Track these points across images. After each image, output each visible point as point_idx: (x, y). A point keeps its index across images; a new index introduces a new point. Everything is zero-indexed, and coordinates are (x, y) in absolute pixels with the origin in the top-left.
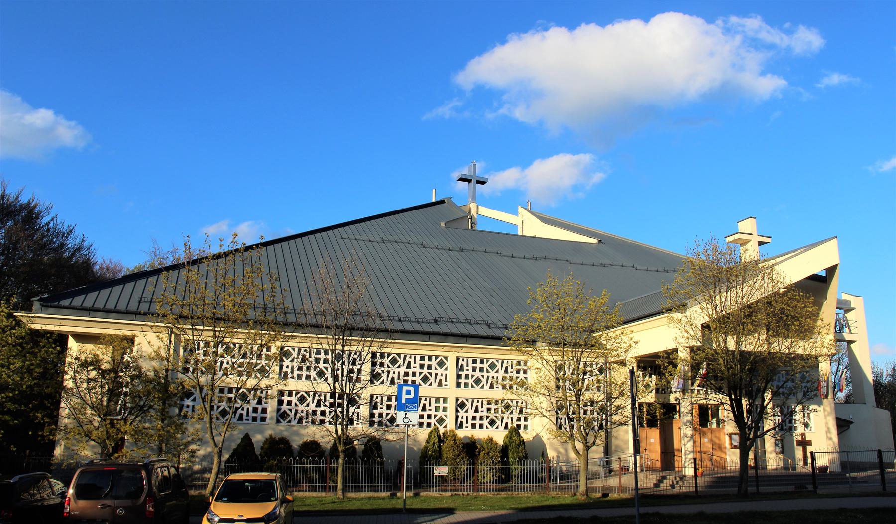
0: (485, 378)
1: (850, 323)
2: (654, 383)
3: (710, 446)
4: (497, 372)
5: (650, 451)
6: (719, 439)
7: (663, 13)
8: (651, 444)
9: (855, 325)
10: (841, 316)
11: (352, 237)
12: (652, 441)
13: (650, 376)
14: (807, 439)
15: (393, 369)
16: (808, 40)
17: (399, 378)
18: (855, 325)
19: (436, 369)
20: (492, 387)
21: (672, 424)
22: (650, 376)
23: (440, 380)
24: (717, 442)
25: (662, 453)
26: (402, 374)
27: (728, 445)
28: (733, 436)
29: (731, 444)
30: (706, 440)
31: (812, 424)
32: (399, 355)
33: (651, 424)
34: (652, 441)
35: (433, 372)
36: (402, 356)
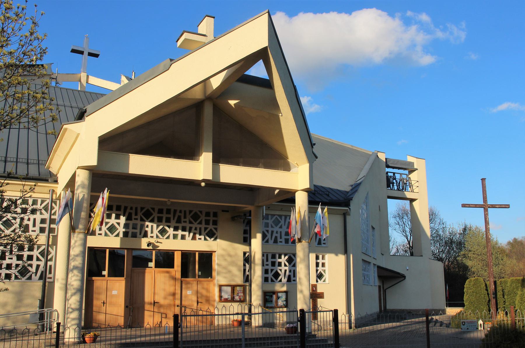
0: (270, 232)
1: (413, 182)
2: (122, 225)
3: (194, 298)
4: (281, 227)
5: (111, 303)
6: (208, 290)
7: (327, 12)
8: (113, 296)
9: (417, 184)
10: (404, 176)
11: (67, 103)
12: (114, 292)
13: (118, 217)
14: (319, 291)
15: (276, 229)
16: (459, 34)
17: (34, 225)
18: (417, 184)
19: (272, 227)
20: (276, 241)
21: (144, 273)
22: (118, 217)
23: (276, 237)
24: (204, 292)
25: (126, 307)
26: (38, 222)
27: (217, 298)
28: (223, 288)
29: (221, 297)
30: (189, 292)
31: (326, 276)
32: (280, 216)
33: (116, 272)
34: (114, 292)
35: (270, 229)
36: (283, 217)
